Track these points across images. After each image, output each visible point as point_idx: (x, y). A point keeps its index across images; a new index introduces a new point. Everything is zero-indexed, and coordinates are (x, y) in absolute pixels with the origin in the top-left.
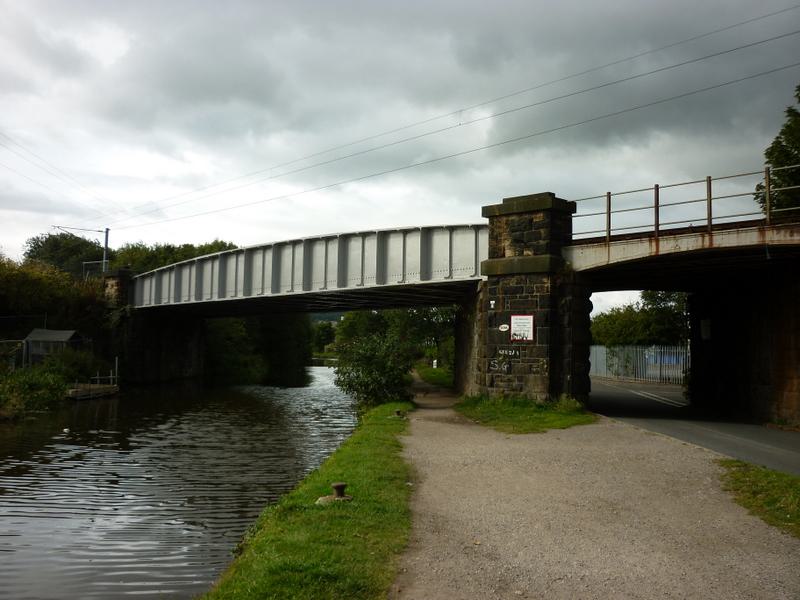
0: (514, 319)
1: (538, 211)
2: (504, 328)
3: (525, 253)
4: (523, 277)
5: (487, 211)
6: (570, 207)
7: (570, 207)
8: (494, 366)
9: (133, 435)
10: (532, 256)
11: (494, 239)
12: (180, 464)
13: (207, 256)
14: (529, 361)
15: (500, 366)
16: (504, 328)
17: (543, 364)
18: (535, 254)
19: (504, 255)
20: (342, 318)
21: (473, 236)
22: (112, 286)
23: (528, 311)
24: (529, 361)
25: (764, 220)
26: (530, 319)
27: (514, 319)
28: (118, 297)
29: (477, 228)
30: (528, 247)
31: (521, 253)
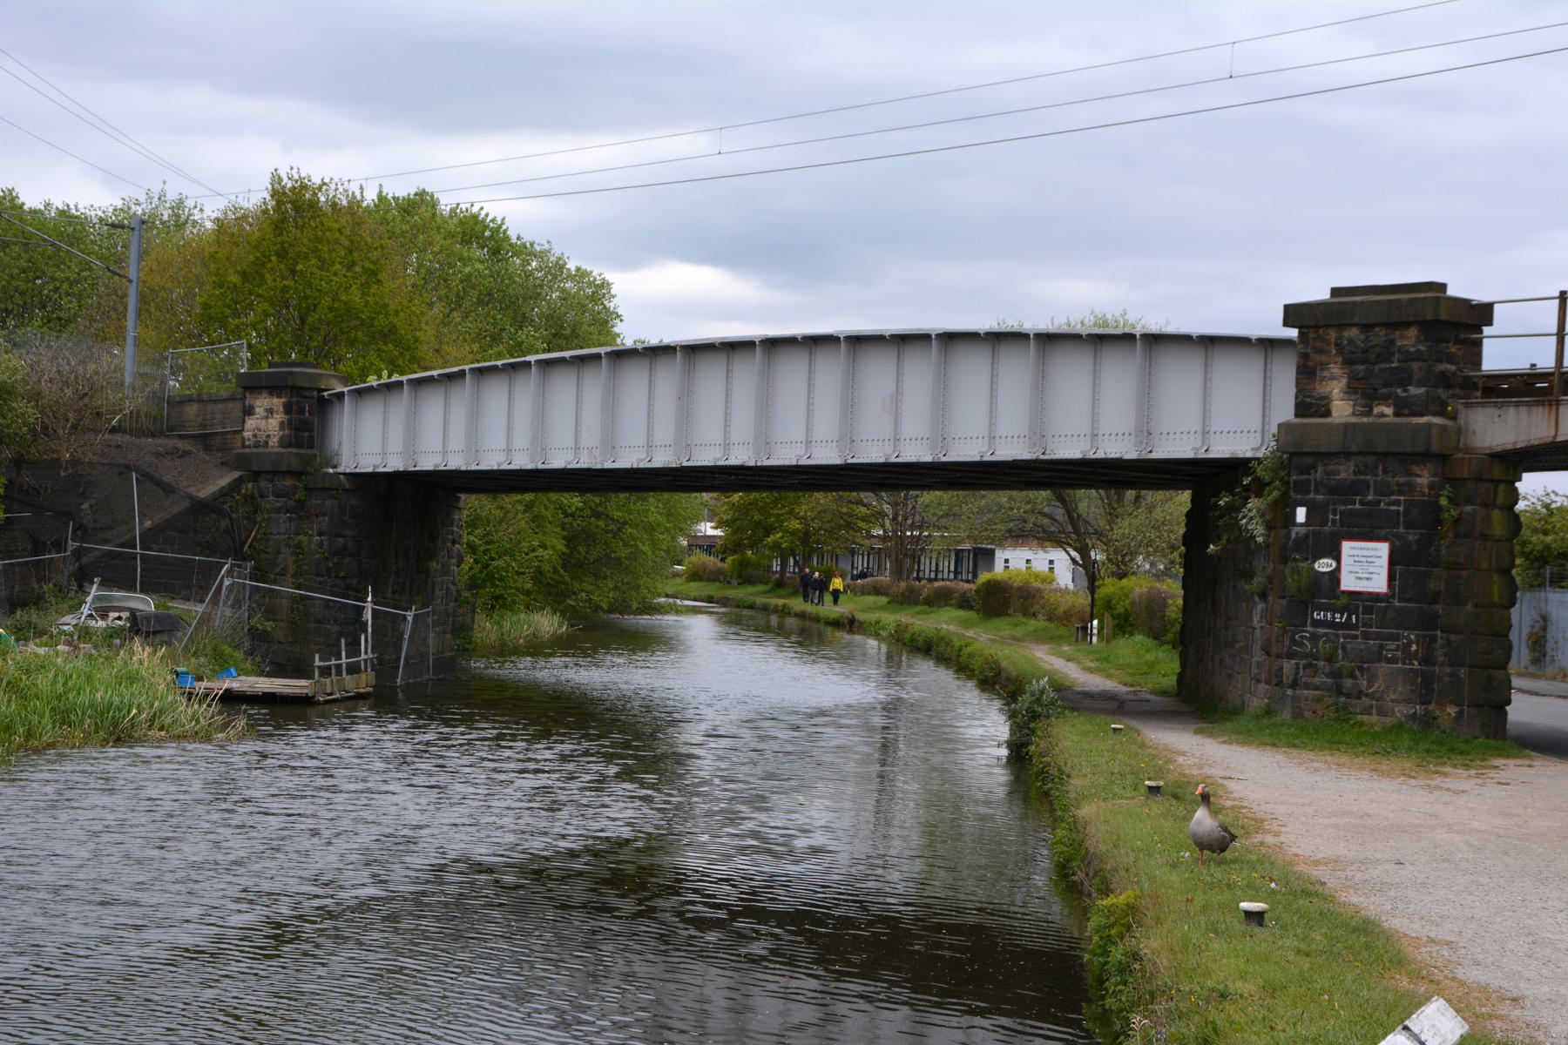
0: (1347, 547)
1: (1407, 325)
2: (1324, 565)
3: (1376, 410)
4: (1370, 460)
5: (1293, 314)
6: (1482, 313)
7: (1482, 313)
8: (1302, 645)
9: (218, 708)
10: (1392, 419)
11: (1307, 373)
12: (723, 840)
13: (567, 354)
14: (1378, 636)
15: (1315, 645)
16: (1324, 565)
17: (1410, 644)
18: (1396, 414)
19: (1327, 413)
20: (1301, 514)
21: (1263, 360)
22: (270, 411)
23: (1382, 533)
24: (1378, 636)
25: (240, 477)
26: (1382, 549)
27: (1347, 547)
28: (1299, 337)
29: (1268, 345)
30: (1385, 399)
31: (1369, 413)
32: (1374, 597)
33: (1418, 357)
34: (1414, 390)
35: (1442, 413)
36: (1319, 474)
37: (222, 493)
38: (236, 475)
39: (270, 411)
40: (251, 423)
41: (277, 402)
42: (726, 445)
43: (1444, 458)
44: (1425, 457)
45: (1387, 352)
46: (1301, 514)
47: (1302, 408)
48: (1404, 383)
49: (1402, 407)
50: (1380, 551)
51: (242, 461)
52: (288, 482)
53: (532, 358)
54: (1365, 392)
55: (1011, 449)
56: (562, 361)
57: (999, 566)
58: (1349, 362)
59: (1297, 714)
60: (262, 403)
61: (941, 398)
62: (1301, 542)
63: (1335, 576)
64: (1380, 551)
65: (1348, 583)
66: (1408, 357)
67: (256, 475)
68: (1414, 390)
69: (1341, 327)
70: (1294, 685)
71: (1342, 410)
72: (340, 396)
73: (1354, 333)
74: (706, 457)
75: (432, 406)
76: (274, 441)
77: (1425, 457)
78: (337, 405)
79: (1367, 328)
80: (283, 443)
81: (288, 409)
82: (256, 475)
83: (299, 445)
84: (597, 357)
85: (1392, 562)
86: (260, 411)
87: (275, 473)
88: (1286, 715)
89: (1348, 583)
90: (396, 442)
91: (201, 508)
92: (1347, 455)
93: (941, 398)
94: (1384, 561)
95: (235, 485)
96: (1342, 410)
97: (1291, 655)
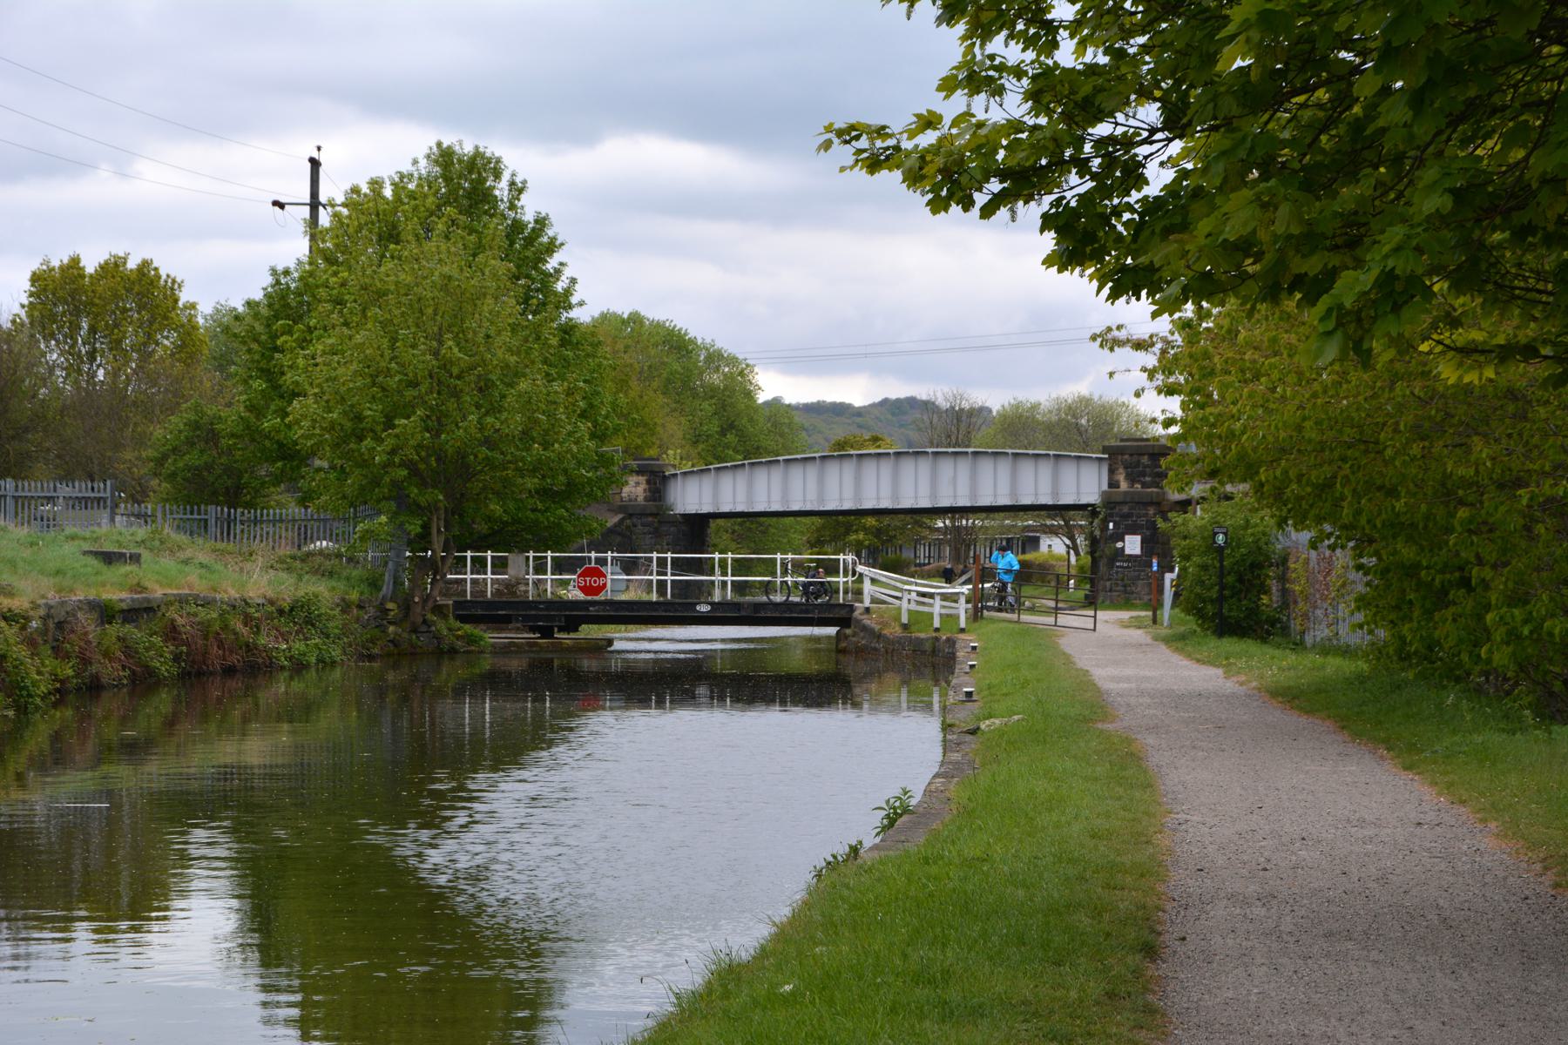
2: (1119, 545)
11: (1111, 472)
16: (1119, 545)
20: (1111, 525)
22: (637, 484)
30: (1138, 482)
32: (1136, 556)
33: (1148, 466)
34: (1148, 479)
35: (1157, 487)
36: (1117, 510)
37: (615, 525)
38: (620, 516)
39: (637, 484)
40: (626, 490)
41: (642, 479)
42: (841, 500)
43: (1158, 504)
44: (1152, 503)
45: (1138, 464)
46: (1111, 525)
47: (1110, 485)
48: (1144, 476)
49: (1144, 485)
50: (1138, 538)
51: (621, 509)
52: (650, 519)
53: (781, 458)
54: (1131, 479)
55: (1004, 501)
56: (796, 460)
57: (1043, 547)
58: (1126, 468)
59: (1112, 602)
60: (632, 480)
61: (750, 485)
62: (1112, 535)
63: (1123, 549)
64: (1138, 538)
65: (1128, 551)
66: (1145, 467)
67: (631, 516)
68: (1148, 479)
69: (1122, 454)
70: (1111, 590)
71: (1124, 486)
72: (675, 475)
73: (1126, 457)
74: (1027, 500)
75: (761, 476)
76: (641, 498)
77: (1152, 503)
78: (672, 480)
79: (1131, 455)
80: (646, 499)
81: (648, 482)
82: (631, 516)
83: (655, 500)
84: (814, 458)
85: (1142, 542)
86: (632, 483)
87: (643, 515)
88: (1108, 602)
89: (1128, 551)
90: (848, 492)
91: (611, 531)
92: (1126, 503)
93: (750, 485)
94: (1139, 543)
95: (622, 521)
96: (1124, 486)
97: (1109, 580)
